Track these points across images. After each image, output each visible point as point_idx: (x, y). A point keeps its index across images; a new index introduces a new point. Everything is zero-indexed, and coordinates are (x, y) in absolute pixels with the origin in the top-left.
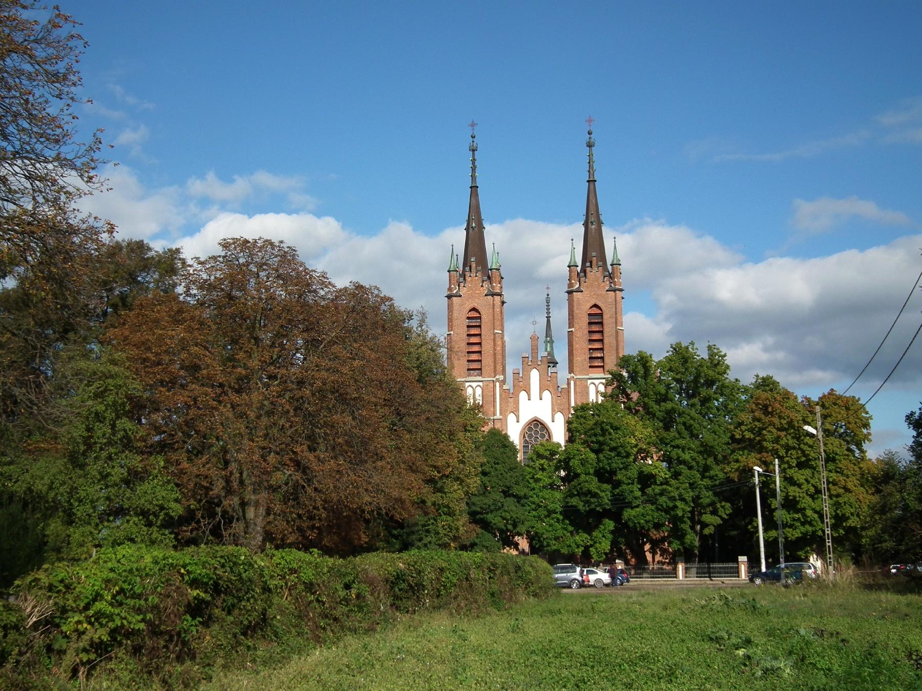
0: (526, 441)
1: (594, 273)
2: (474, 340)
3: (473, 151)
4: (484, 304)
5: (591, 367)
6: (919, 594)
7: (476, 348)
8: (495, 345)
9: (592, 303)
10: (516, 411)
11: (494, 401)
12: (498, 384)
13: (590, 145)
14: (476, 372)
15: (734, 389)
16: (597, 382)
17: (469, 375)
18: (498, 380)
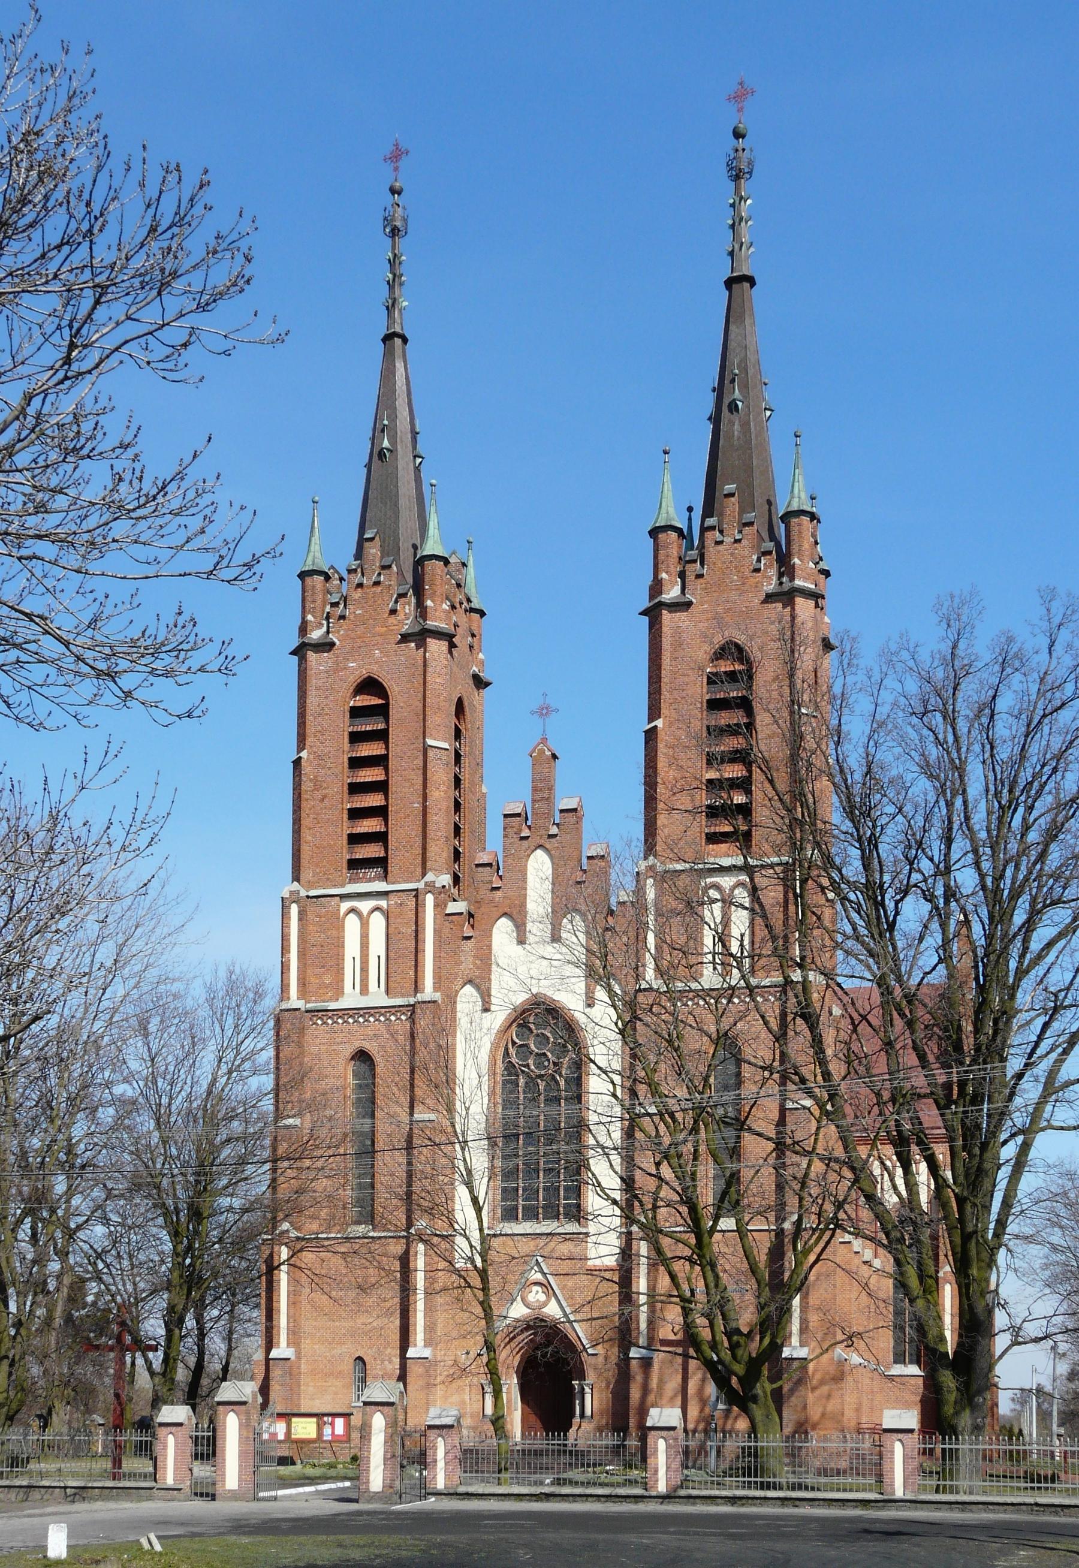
0: (510, 1067)
1: (735, 553)
3: (395, 232)
4: (392, 665)
7: (374, 800)
11: (418, 951)
12: (430, 899)
13: (737, 176)
14: (372, 873)
15: (65, 1560)
16: (365, 906)
18: (430, 887)
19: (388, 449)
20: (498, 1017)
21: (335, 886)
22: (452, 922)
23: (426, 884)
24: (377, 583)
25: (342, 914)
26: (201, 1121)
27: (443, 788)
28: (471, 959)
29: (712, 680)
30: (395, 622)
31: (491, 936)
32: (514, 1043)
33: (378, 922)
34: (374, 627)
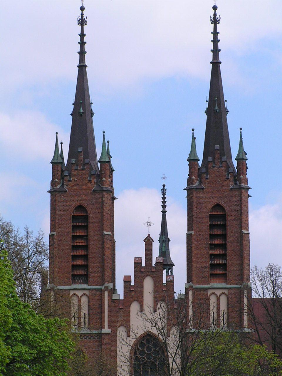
2: (79, 243)
5: (212, 275)
6: (131, 374)
8: (103, 248)
9: (215, 202)
10: (127, 324)
12: (106, 294)
17: (74, 283)
18: (107, 288)
19: (82, 112)
20: (132, 340)
21: (67, 285)
22: (115, 302)
23: (105, 287)
24: (83, 169)
25: (70, 296)
26: (26, 301)
27: (110, 250)
28: (122, 317)
29: (212, 216)
30: (91, 185)
31: (130, 309)
32: (138, 349)
33: (84, 300)
34: (82, 186)
